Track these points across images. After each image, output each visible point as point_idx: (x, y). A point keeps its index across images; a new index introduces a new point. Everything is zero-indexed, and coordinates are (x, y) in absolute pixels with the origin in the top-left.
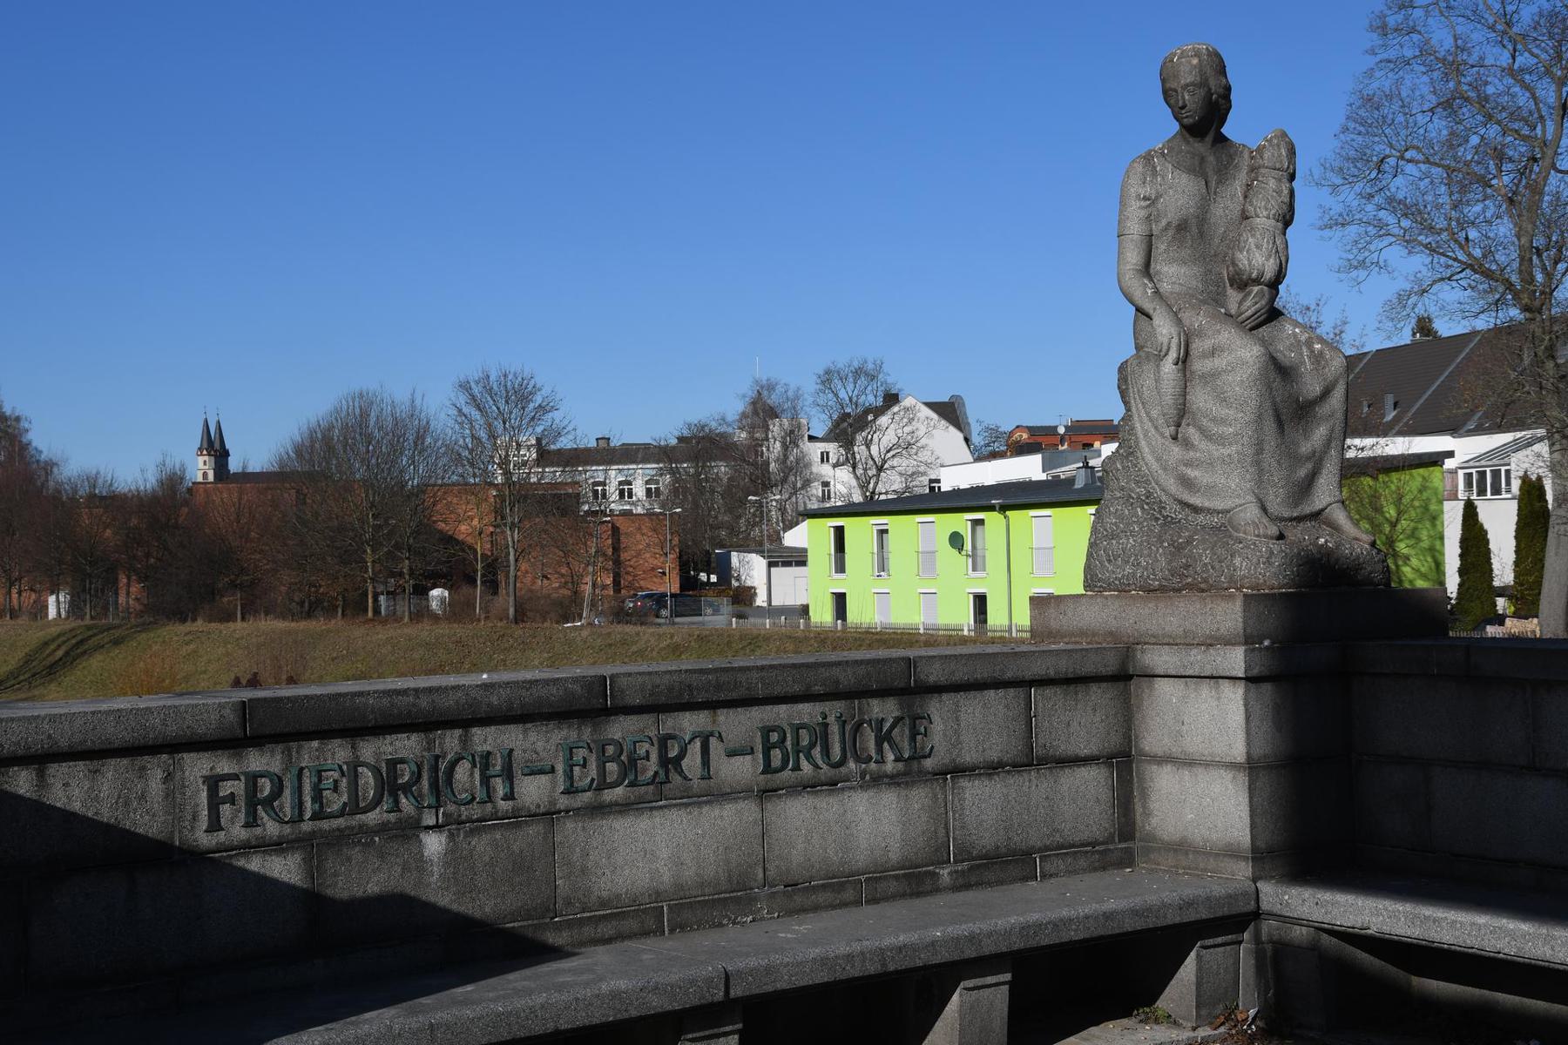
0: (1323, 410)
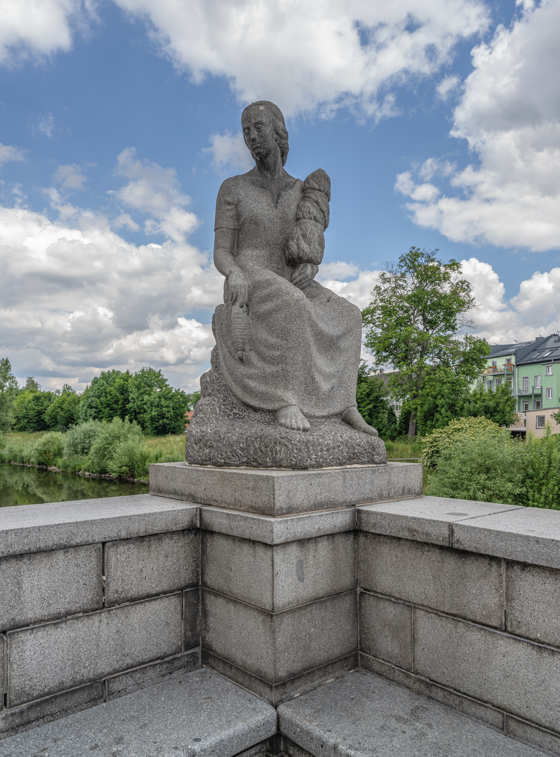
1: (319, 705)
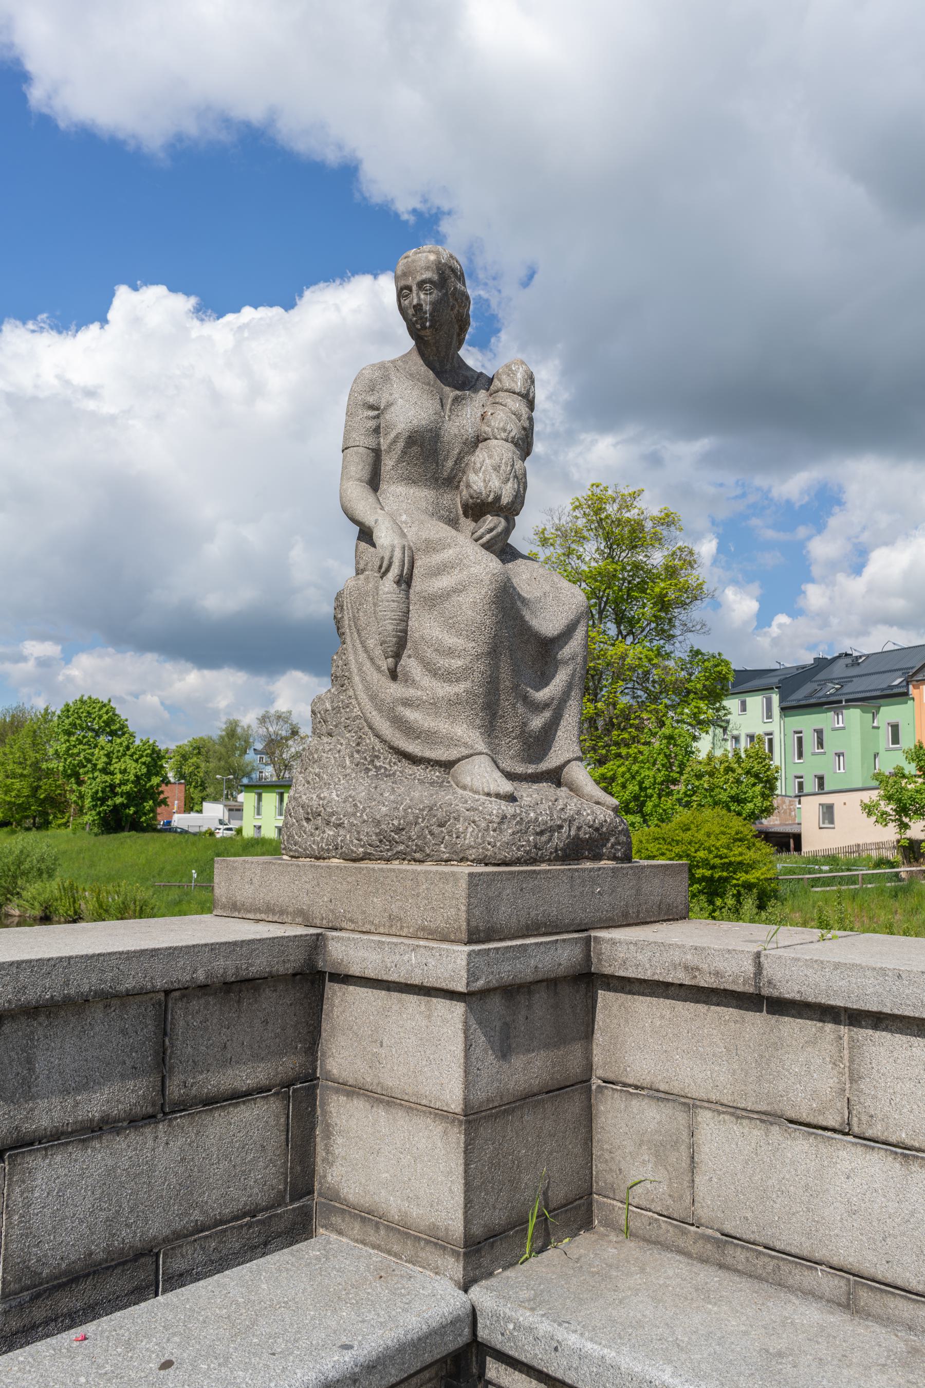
0: (566, 652)
1: (540, 1284)
